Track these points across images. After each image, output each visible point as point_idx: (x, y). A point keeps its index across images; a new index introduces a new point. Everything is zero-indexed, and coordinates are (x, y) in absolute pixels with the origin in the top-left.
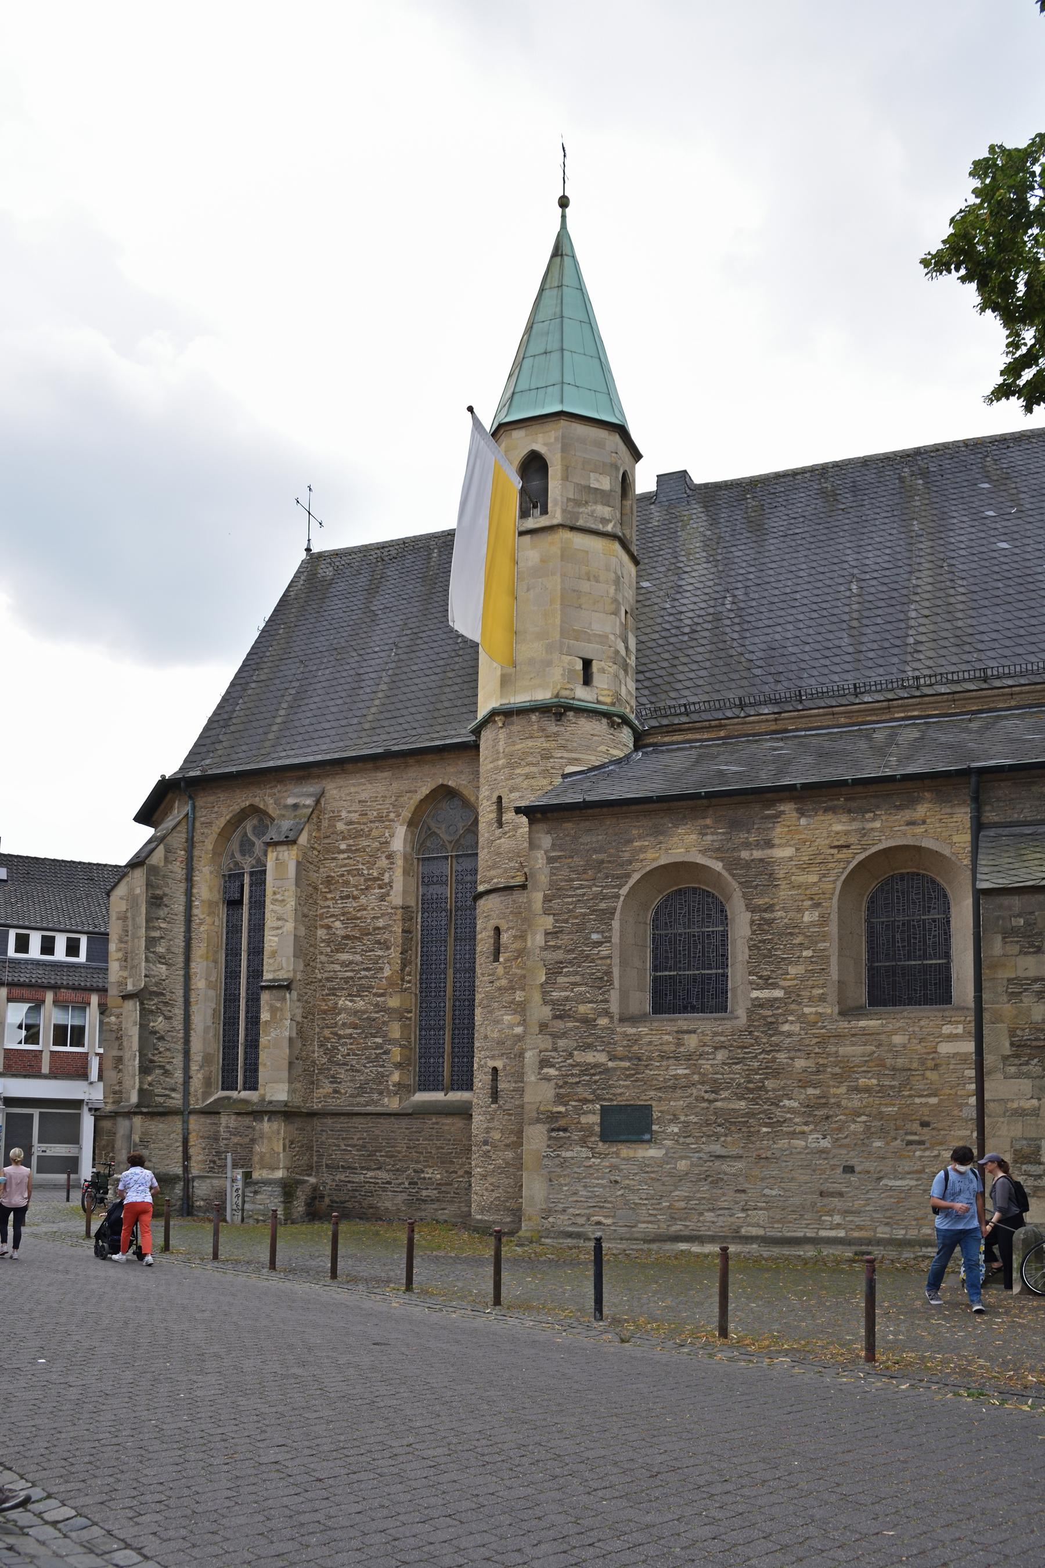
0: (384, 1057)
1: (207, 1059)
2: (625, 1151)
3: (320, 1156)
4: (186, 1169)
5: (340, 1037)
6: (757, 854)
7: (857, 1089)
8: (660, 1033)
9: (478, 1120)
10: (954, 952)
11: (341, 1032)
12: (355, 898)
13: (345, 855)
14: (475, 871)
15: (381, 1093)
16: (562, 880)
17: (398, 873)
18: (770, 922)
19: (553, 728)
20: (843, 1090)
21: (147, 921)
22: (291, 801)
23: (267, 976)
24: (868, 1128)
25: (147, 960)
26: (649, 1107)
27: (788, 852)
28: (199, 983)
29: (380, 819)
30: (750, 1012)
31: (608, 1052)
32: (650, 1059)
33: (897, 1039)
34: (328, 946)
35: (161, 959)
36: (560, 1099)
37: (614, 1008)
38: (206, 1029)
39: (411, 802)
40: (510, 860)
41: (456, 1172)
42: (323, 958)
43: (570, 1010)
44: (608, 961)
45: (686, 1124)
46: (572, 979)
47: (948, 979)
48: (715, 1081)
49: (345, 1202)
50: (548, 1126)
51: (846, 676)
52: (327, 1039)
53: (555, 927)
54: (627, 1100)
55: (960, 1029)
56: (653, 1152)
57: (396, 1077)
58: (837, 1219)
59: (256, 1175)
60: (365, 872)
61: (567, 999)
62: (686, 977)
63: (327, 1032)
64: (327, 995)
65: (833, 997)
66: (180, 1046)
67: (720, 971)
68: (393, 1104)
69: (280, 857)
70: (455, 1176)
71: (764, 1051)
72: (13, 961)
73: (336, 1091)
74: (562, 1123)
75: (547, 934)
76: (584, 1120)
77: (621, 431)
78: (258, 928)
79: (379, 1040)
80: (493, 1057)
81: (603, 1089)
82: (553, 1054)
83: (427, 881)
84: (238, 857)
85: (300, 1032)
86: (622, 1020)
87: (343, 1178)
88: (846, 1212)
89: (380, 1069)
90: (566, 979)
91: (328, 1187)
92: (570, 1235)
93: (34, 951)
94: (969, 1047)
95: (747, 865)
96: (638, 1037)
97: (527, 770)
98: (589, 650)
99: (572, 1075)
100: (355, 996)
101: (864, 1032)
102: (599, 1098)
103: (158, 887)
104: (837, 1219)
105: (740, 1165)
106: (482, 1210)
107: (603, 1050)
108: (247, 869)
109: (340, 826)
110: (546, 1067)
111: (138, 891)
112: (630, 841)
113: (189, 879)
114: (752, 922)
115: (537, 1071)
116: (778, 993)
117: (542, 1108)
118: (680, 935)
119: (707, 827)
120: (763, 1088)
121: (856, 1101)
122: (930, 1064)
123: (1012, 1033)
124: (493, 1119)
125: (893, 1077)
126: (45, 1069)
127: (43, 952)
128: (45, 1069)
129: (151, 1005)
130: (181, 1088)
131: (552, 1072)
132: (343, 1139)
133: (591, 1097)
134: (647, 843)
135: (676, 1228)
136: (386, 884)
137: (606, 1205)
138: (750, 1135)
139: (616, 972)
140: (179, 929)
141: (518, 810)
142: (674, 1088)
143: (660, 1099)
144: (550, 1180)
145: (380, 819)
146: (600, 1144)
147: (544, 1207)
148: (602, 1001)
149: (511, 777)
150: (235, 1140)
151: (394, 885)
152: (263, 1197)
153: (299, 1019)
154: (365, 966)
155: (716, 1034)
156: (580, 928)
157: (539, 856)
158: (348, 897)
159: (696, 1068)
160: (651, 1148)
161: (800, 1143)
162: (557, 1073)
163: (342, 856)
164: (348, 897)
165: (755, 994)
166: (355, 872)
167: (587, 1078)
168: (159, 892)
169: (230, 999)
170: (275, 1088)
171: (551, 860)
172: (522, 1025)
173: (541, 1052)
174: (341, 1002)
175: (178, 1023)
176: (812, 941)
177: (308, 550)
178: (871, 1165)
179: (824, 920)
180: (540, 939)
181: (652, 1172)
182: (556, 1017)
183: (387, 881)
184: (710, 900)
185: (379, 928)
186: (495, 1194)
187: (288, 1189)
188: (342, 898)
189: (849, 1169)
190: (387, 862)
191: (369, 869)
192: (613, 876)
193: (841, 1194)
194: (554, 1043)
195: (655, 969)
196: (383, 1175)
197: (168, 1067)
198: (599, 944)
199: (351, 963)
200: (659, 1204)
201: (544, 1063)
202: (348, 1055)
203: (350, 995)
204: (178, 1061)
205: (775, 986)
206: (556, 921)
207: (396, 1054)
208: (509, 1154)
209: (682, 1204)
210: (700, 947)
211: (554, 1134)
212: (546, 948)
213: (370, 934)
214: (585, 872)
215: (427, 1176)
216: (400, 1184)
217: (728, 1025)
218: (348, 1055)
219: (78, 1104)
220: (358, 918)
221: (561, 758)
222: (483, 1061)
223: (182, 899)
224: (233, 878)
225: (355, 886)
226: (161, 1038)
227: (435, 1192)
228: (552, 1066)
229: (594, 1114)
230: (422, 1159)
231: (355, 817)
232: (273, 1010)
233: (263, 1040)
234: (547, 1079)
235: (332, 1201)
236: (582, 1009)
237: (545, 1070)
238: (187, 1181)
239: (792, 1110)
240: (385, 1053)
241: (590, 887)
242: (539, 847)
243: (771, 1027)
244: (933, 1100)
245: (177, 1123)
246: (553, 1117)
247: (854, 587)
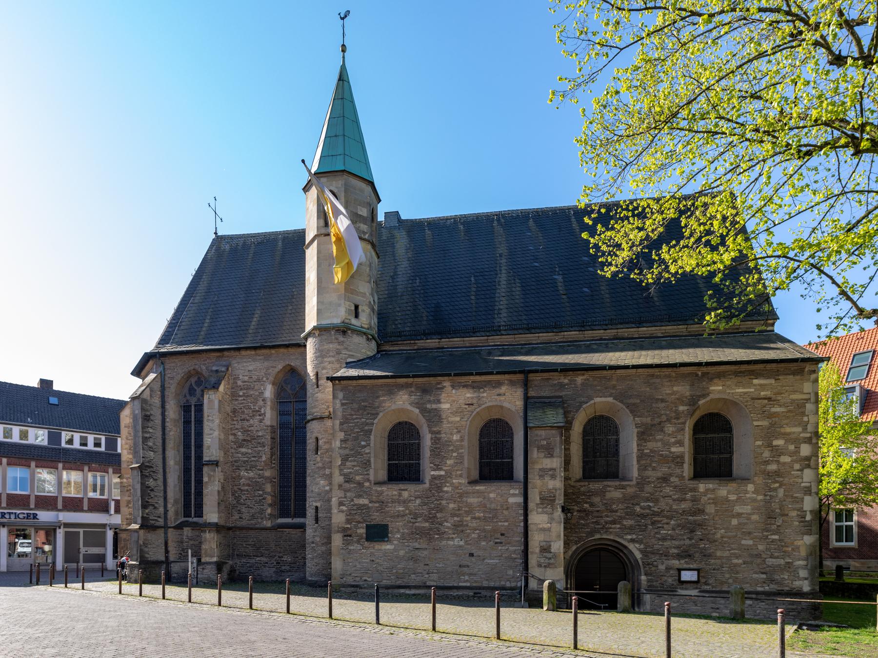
1: (176, 502)
3: (234, 550)
4: (167, 558)
5: (242, 490)
6: (434, 406)
7: (475, 518)
8: (391, 491)
9: (309, 532)
10: (515, 456)
12: (248, 420)
14: (305, 409)
15: (262, 519)
17: (268, 408)
18: (439, 439)
19: (341, 338)
20: (469, 518)
21: (143, 428)
22: (214, 368)
23: (206, 458)
24: (479, 536)
25: (143, 449)
27: (447, 406)
28: (171, 462)
29: (258, 380)
30: (431, 482)
32: (388, 502)
33: (492, 495)
35: (151, 449)
36: (348, 521)
37: (372, 478)
38: (175, 486)
39: (274, 372)
42: (233, 451)
45: (403, 534)
46: (353, 464)
47: (512, 468)
51: (469, 323)
52: (236, 492)
55: (517, 492)
56: (389, 547)
57: (269, 511)
58: (467, 578)
59: (203, 560)
61: (350, 473)
62: (403, 465)
63: (235, 488)
65: (465, 475)
66: (162, 494)
68: (268, 524)
71: (436, 500)
72: (64, 449)
73: (241, 518)
74: (349, 533)
75: (341, 441)
76: (359, 531)
77: (372, 184)
78: (200, 434)
79: (261, 492)
80: (316, 501)
83: (282, 413)
84: (188, 397)
85: (223, 488)
86: (375, 484)
88: (470, 574)
92: (353, 586)
93: (91, 439)
94: (520, 500)
95: (430, 411)
96: (382, 492)
97: (329, 359)
98: (358, 299)
101: (478, 492)
102: (365, 521)
103: (147, 410)
104: (467, 578)
105: (426, 552)
106: (311, 576)
108: (193, 403)
109: (239, 383)
111: (137, 412)
112: (378, 397)
113: (163, 407)
114: (432, 439)
116: (442, 473)
119: (412, 392)
120: (435, 517)
121: (474, 524)
122: (505, 507)
123: (540, 493)
125: (490, 513)
126: (86, 508)
127: (81, 444)
128: (86, 508)
129: (146, 473)
130: (163, 516)
131: (344, 508)
135: (399, 582)
138: (430, 539)
139: (372, 460)
140: (159, 434)
141: (328, 378)
142: (398, 516)
145: (258, 380)
150: (192, 542)
153: (222, 481)
155: (416, 491)
156: (356, 439)
158: (244, 420)
159: (407, 508)
161: (451, 543)
164: (244, 420)
165: (433, 473)
168: (148, 413)
169: (186, 470)
170: (211, 515)
171: (343, 404)
175: (160, 482)
176: (457, 449)
177: (216, 233)
178: (480, 553)
179: (462, 440)
180: (338, 444)
182: (346, 482)
187: (219, 566)
189: (471, 555)
193: (468, 566)
195: (389, 460)
196: (264, 559)
197: (156, 505)
198: (364, 447)
201: (341, 504)
204: (161, 502)
205: (441, 469)
207: (269, 499)
208: (324, 548)
212: (341, 448)
217: (421, 487)
219: (104, 526)
222: (311, 503)
223: (160, 417)
224: (186, 409)
226: (152, 490)
228: (344, 505)
231: (246, 378)
232: (210, 477)
233: (205, 491)
234: (342, 511)
236: (358, 478)
238: (167, 562)
239: (448, 528)
242: (337, 398)
243: (439, 488)
244: (506, 524)
245: (161, 532)
246: (344, 530)
247: (472, 279)
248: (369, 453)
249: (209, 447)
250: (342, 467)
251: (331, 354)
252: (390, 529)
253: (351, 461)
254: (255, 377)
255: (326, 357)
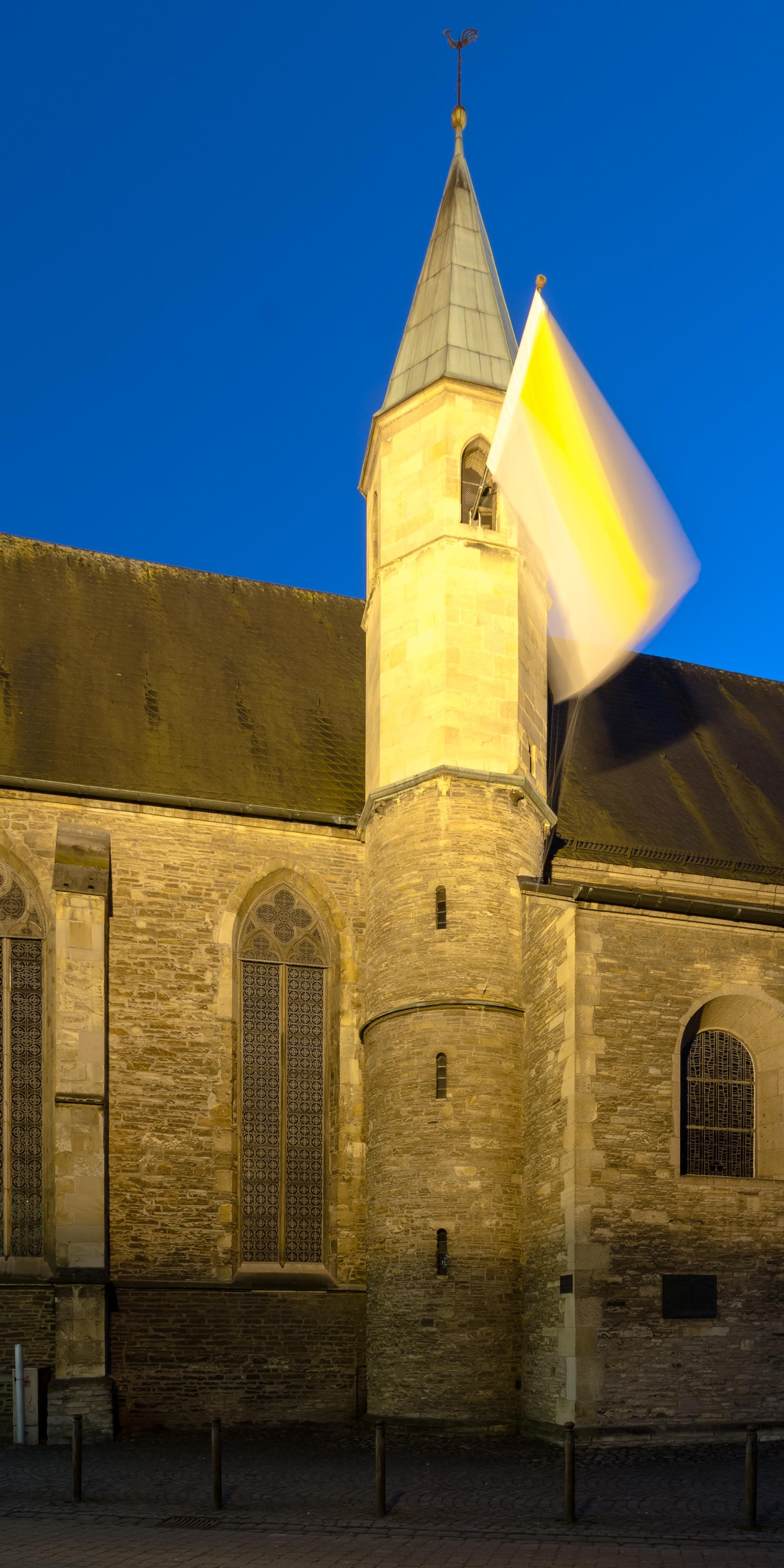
0: (210, 1215)
2: (689, 1329)
5: (145, 1185)
11: (146, 1178)
12: (163, 998)
13: (146, 938)
16: (615, 995)
26: (713, 1279)
31: (668, 1212)
34: (123, 1059)
36: (617, 1267)
40: (460, 971)
41: (309, 1361)
43: (626, 1158)
44: (668, 1103)
46: (630, 1120)
48: (778, 1250)
49: (157, 1404)
50: (602, 1300)
53: (607, 1053)
54: (689, 1270)
56: (715, 1331)
59: (62, 1374)
60: (178, 965)
61: (622, 1143)
64: (123, 1127)
67: (746, 1130)
69: (78, 914)
70: (307, 1366)
74: (618, 1296)
75: (599, 1060)
76: (643, 1292)
80: (438, 1217)
81: (664, 1256)
82: (608, 1211)
87: (152, 1373)
89: (204, 1231)
90: (621, 1120)
91: (130, 1387)
97: (480, 859)
99: (630, 1237)
100: (167, 1132)
102: (659, 1267)
107: (664, 1210)
110: (599, 1226)
112: (690, 961)
115: (589, 1232)
117: (596, 1278)
118: (707, 1084)
119: (768, 960)
124: (441, 1293)
132: (151, 1321)
133: (651, 1265)
134: (708, 967)
136: (207, 987)
137: (669, 1393)
143: (724, 1270)
144: (607, 1366)
145: (195, 896)
146: (662, 1321)
147: (599, 1399)
148: (661, 1151)
149: (459, 865)
151: (220, 989)
152: (78, 1404)
154: (181, 1093)
156: (636, 1058)
157: (588, 959)
158: (151, 996)
160: (714, 1325)
162: (612, 1235)
163: (139, 938)
164: (151, 996)
166: (162, 963)
167: (647, 1242)
171: (602, 967)
172: (479, 1179)
173: (593, 1207)
174: (145, 1138)
181: (716, 1353)
182: (613, 1166)
183: (208, 981)
184: (737, 1049)
185: (198, 1044)
186: (445, 1387)
188: (141, 996)
190: (209, 957)
191: (181, 961)
192: (673, 999)
194: (609, 1198)
196: (211, 1368)
198: (657, 1080)
199: (159, 1086)
200: (723, 1390)
202: (158, 1209)
203: (158, 1130)
206: (610, 1045)
209: (746, 1389)
210: (726, 1100)
211: (610, 1309)
212: (597, 1078)
213: (186, 1050)
214: (641, 989)
215: (272, 1367)
216: (235, 1379)
218: (158, 1209)
220: (169, 1027)
221: (516, 855)
225: (163, 983)
227: (282, 1387)
228: (606, 1225)
229: (654, 1285)
230: (264, 1345)
231: (159, 886)
235: (137, 1405)
236: (641, 1158)
237: (599, 1231)
240: (211, 1210)
241: (647, 1009)
242: (588, 949)
248: (669, 1098)
249: (72, 1057)
250: (601, 1128)
251: (484, 847)
252: (720, 1287)
253: (623, 1114)
254: (185, 887)
255: (471, 852)
